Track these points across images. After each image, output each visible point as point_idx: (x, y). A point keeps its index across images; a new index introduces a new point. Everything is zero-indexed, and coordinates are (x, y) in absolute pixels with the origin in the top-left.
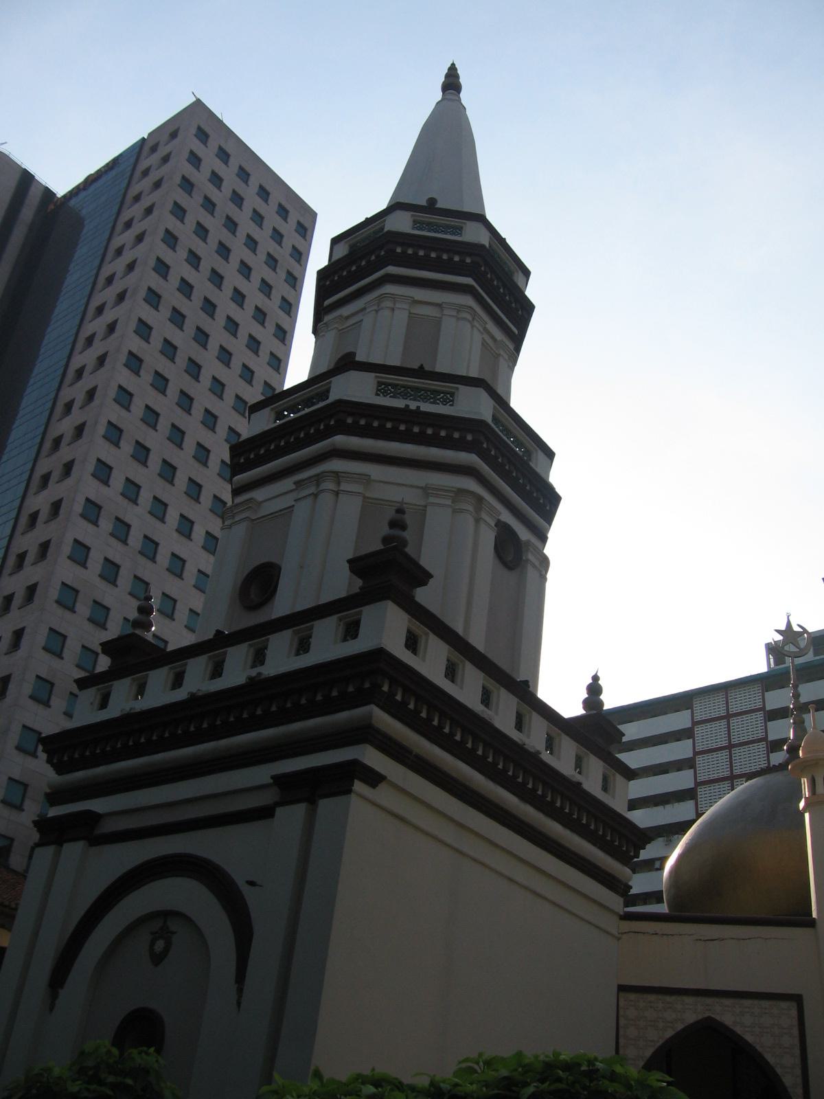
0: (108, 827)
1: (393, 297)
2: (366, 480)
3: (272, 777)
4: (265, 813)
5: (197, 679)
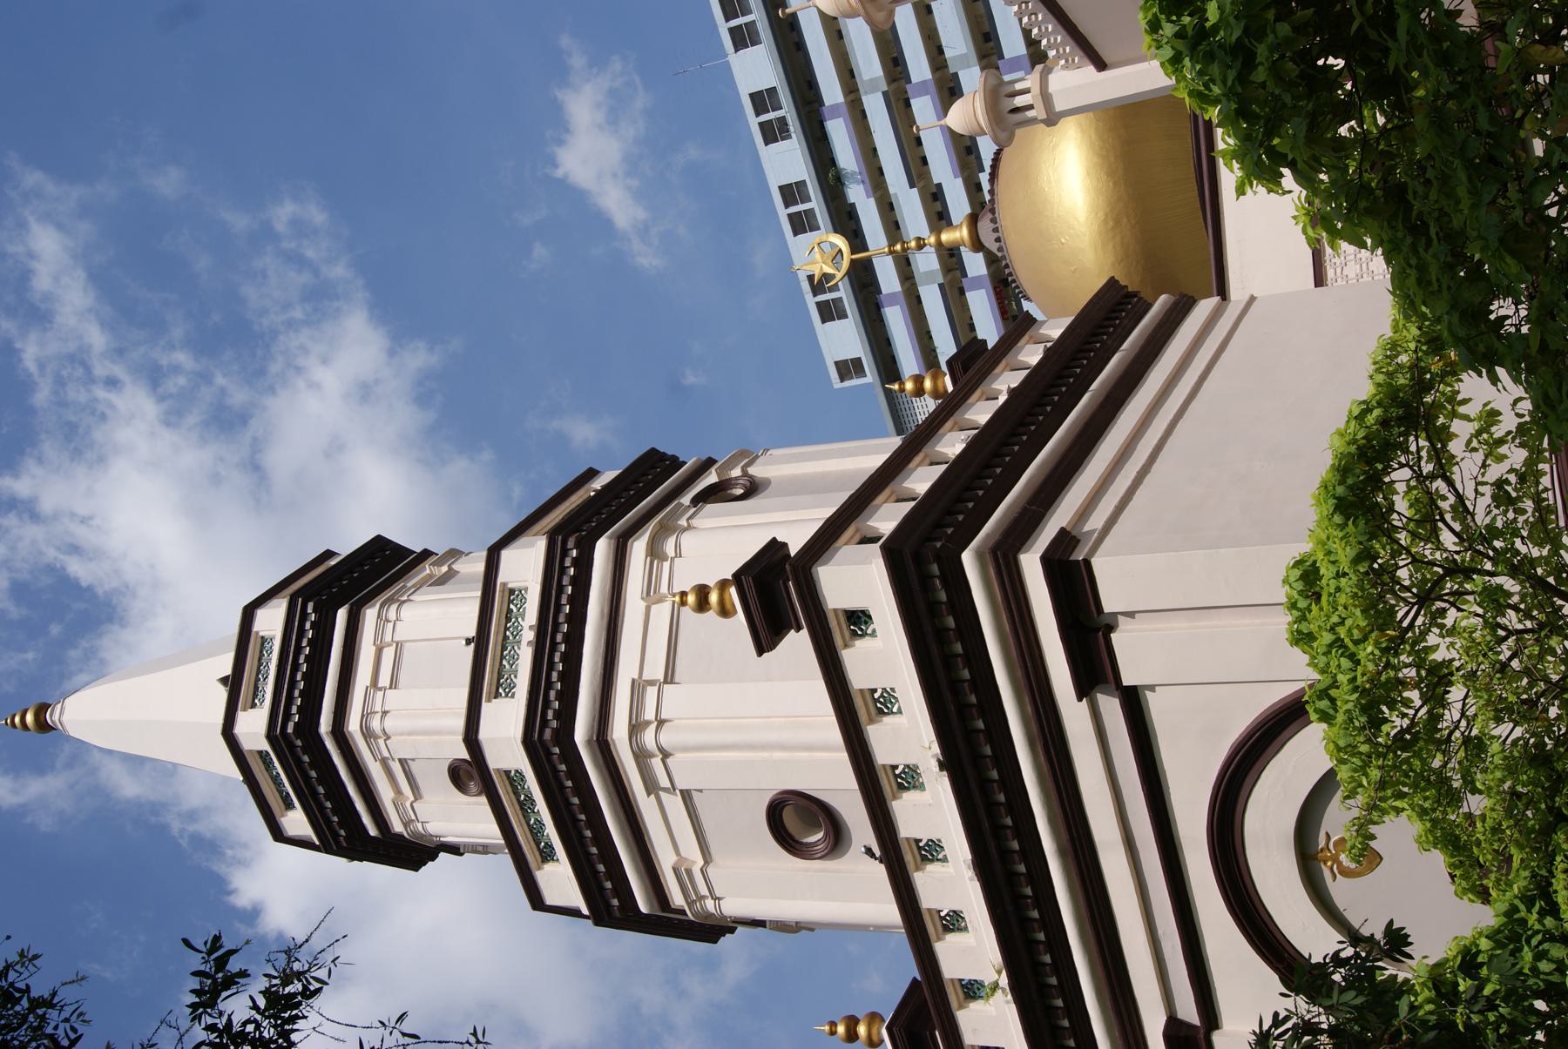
0: (1188, 1011)
1: (366, 716)
2: (638, 688)
3: (1080, 700)
4: (1133, 702)
5: (952, 883)
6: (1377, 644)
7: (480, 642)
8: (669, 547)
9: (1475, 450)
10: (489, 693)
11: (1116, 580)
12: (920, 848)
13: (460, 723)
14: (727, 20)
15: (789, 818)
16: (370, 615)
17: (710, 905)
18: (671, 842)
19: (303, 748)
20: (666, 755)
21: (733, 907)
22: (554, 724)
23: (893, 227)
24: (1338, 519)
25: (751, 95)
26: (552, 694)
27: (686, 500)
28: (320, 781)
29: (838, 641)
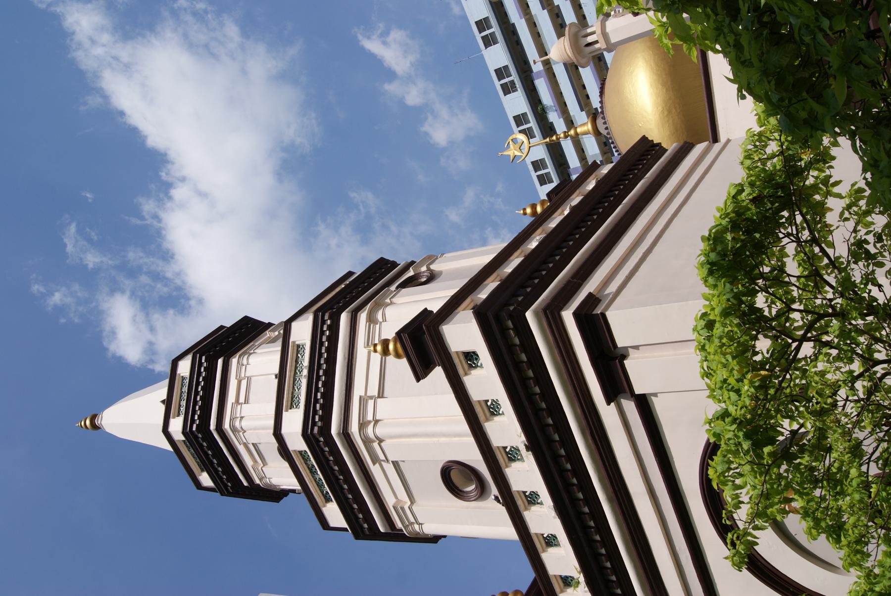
1: (232, 420)
2: (363, 401)
3: (609, 404)
4: (644, 404)
5: (544, 519)
6: (751, 382)
7: (281, 377)
8: (379, 316)
9: (847, 219)
10: (287, 406)
11: (623, 325)
12: (526, 496)
13: (271, 422)
14: (480, 33)
15: (455, 476)
16: (234, 361)
17: (417, 527)
18: (392, 494)
19: (202, 438)
20: (381, 441)
21: (430, 529)
22: (320, 424)
23: (537, 36)
24: (711, 280)
25: (496, 71)
26: (318, 406)
27: (393, 288)
28: (214, 456)
29: (461, 371)
